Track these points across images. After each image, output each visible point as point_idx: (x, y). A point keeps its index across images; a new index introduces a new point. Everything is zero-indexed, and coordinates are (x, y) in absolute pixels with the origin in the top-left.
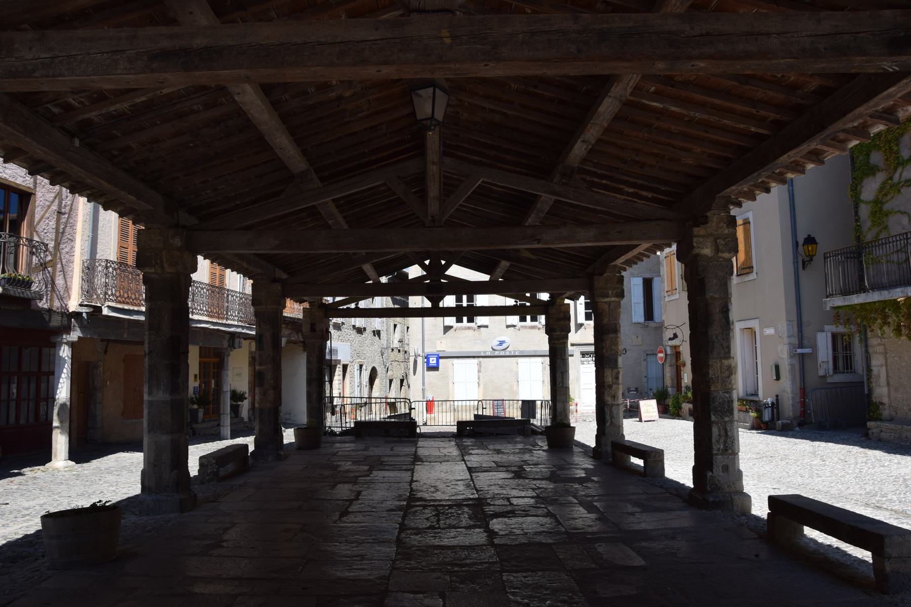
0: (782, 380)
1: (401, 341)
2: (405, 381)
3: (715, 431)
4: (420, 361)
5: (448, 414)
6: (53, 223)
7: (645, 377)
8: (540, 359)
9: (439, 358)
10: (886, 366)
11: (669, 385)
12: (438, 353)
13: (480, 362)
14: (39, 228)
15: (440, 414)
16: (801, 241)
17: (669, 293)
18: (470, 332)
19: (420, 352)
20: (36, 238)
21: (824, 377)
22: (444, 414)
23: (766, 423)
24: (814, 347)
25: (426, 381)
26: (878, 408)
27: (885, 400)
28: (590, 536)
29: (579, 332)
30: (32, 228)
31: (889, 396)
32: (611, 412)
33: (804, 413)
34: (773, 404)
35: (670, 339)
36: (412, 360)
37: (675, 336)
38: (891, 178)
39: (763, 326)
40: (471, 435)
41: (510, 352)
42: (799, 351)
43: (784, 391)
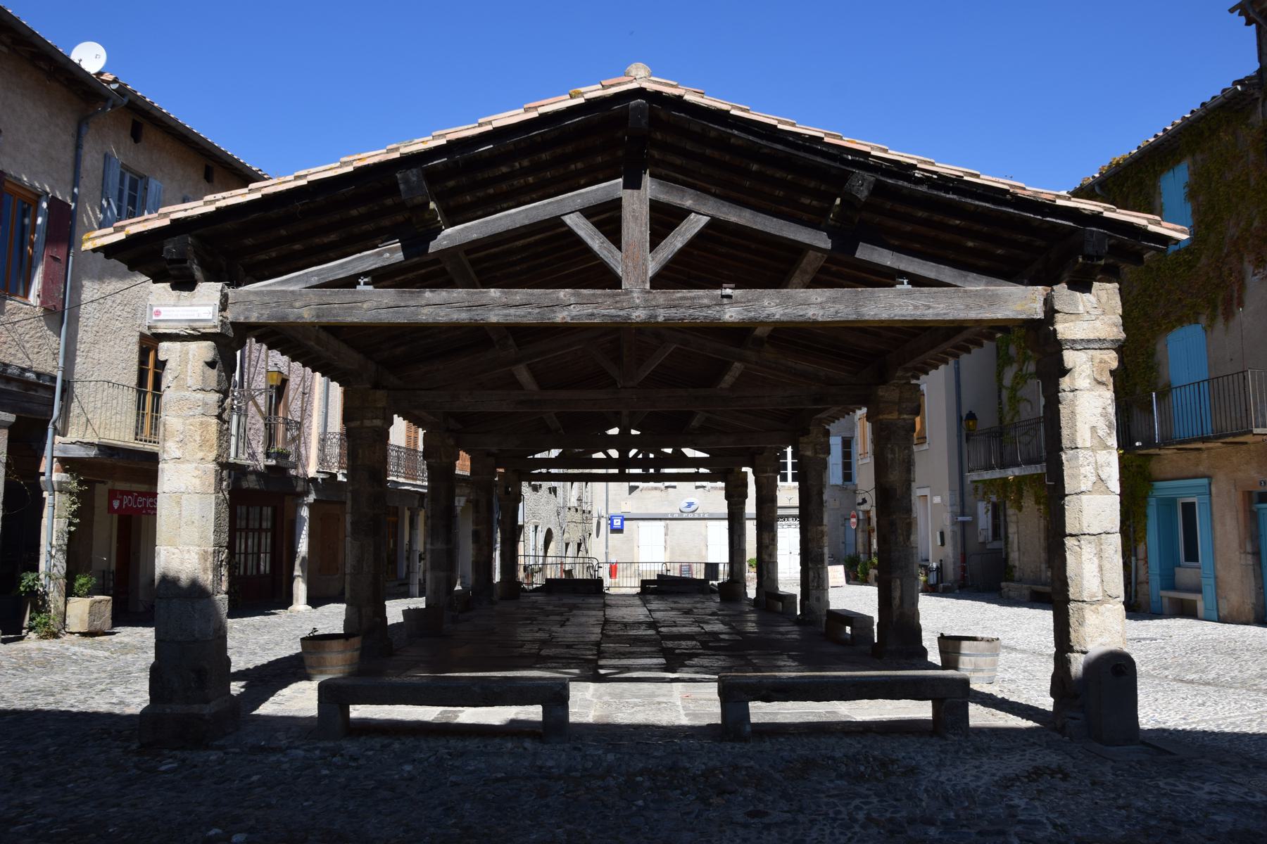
0: (946, 546)
1: (579, 500)
2: (583, 545)
4: (603, 522)
5: (633, 579)
6: (299, 403)
7: (843, 543)
8: (752, 521)
9: (624, 519)
10: (1018, 533)
11: (861, 551)
13: (667, 525)
14: (291, 409)
15: (625, 579)
16: (964, 417)
17: (862, 456)
18: (657, 493)
19: (604, 513)
20: (290, 417)
21: (984, 543)
22: (629, 579)
23: (931, 586)
24: (975, 515)
25: (609, 544)
26: (1012, 571)
27: (1017, 564)
28: (354, 212)
30: (286, 407)
31: (1019, 560)
32: (767, 567)
33: (963, 577)
34: (937, 568)
36: (595, 521)
37: (864, 501)
38: (1021, 370)
39: (933, 495)
40: (653, 592)
41: (699, 514)
42: (960, 519)
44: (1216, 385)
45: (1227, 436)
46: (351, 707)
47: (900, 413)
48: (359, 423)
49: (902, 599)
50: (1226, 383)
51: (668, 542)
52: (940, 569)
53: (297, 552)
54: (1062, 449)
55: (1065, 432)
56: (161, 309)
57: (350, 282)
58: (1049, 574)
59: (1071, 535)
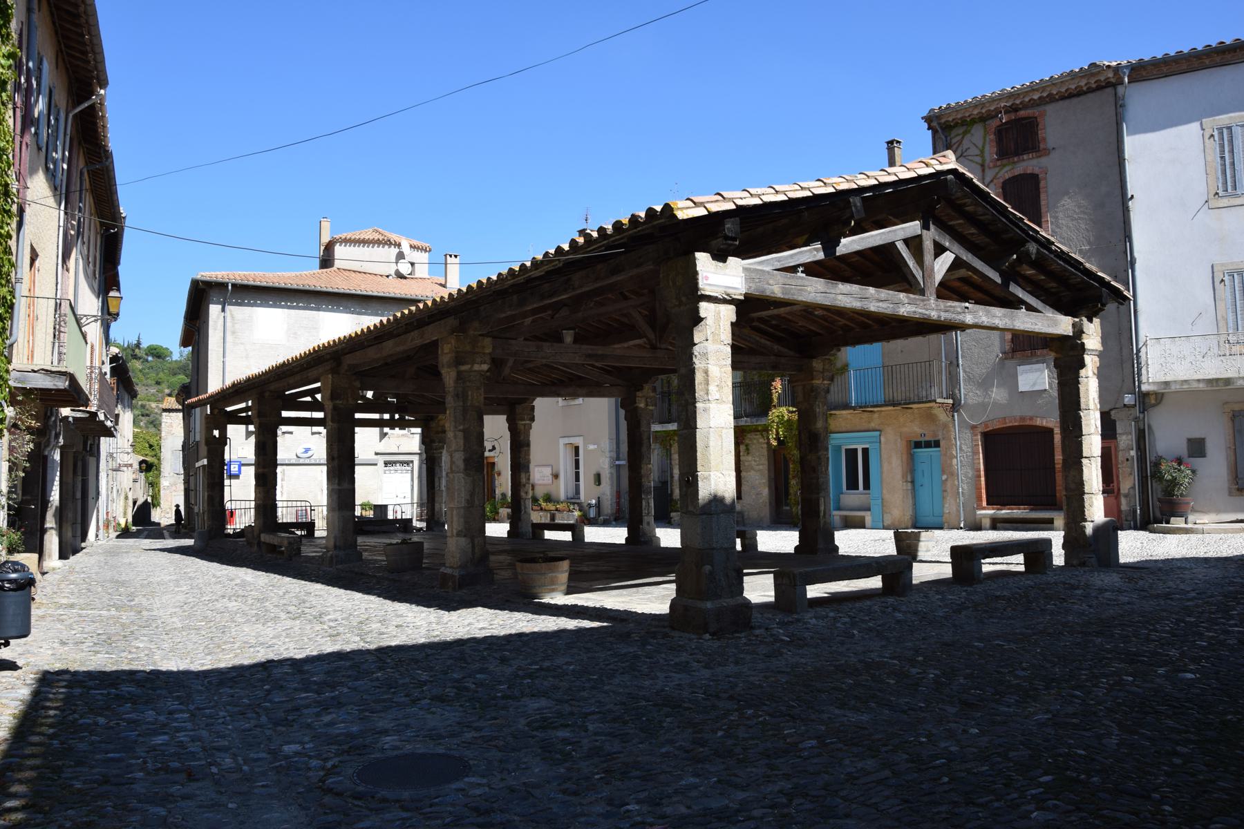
3: (644, 503)
12: (239, 460)
35: (490, 451)
41: (315, 460)
42: (617, 463)
43: (604, 494)
44: (919, 368)
45: (865, 407)
46: (808, 588)
47: (823, 380)
48: (469, 366)
50: (923, 368)
51: (284, 487)
52: (598, 505)
53: (49, 501)
54: (1080, 410)
55: (1082, 400)
56: (709, 275)
57: (792, 269)
58: (231, 532)
59: (1086, 457)
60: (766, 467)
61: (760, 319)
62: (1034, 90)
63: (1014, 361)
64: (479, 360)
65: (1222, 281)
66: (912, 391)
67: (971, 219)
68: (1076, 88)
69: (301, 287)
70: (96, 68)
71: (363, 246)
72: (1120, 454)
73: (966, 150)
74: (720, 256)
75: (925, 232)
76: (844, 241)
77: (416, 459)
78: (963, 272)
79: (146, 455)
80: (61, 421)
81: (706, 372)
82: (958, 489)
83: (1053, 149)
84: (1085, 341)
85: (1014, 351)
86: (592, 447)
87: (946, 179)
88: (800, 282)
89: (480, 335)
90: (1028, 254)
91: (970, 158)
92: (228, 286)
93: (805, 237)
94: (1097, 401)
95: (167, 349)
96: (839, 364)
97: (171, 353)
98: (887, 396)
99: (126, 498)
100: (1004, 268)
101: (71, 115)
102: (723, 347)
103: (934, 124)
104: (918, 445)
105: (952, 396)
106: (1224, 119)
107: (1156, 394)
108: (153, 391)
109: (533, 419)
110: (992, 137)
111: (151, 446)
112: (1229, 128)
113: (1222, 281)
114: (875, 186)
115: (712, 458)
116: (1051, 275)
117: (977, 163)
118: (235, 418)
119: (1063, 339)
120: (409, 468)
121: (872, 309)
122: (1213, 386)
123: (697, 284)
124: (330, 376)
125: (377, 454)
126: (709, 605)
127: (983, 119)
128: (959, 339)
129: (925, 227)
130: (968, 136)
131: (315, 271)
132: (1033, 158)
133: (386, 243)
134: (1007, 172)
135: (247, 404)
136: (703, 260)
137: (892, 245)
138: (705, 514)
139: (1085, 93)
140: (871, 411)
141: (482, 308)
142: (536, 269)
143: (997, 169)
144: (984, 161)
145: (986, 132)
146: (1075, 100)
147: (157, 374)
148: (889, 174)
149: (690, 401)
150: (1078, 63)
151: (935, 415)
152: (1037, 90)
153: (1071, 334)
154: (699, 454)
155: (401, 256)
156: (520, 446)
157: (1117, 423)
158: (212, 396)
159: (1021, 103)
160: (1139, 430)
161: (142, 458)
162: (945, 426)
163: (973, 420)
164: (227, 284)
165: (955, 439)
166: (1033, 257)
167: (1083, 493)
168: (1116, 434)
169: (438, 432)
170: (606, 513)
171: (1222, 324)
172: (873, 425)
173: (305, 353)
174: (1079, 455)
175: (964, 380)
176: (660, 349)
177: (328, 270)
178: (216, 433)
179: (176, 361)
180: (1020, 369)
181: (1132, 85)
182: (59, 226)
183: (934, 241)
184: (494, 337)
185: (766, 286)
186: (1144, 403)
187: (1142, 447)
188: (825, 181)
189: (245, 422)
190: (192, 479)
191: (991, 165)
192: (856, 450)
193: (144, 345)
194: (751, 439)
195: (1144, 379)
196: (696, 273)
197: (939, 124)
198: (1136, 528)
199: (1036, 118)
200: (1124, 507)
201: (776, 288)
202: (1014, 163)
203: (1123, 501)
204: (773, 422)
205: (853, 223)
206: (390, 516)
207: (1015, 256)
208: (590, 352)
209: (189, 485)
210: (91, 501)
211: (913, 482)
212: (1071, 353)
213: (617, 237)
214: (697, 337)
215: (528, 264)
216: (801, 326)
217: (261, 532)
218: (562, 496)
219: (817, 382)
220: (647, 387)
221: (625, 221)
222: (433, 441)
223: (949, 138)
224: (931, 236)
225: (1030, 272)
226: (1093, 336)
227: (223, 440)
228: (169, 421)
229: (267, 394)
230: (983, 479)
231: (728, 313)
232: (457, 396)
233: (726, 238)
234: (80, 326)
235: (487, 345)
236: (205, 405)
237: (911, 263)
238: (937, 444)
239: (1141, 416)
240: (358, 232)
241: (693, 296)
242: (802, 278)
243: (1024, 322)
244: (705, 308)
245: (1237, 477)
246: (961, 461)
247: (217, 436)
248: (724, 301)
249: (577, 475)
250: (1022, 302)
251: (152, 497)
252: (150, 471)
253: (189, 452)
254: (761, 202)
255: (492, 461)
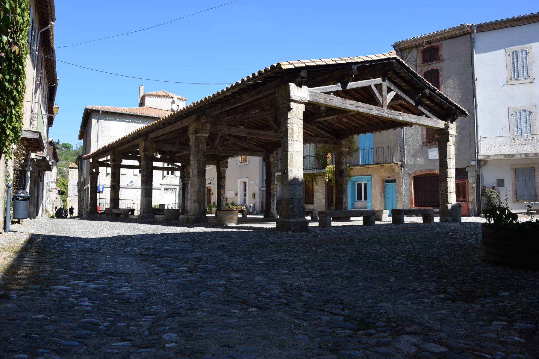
0: (255, 199)
3: (272, 200)
29: (164, 179)
35: (209, 184)
41: (135, 186)
42: (262, 189)
45: (365, 165)
46: (275, 227)
47: (346, 149)
48: (200, 134)
49: (345, 202)
52: (254, 207)
55: (448, 155)
57: (329, 93)
60: (324, 191)
61: (319, 122)
62: (438, 35)
63: (427, 147)
64: (204, 132)
65: (512, 114)
66: (385, 159)
67: (403, 79)
68: (455, 34)
69: (131, 113)
70: (51, 13)
71: (158, 98)
72: (469, 185)
73: (410, 59)
74: (299, 85)
75: (383, 82)
76: (350, 84)
77: (178, 188)
78: (400, 101)
79: (62, 188)
80: (31, 160)
81: (293, 130)
82: (403, 200)
83: (445, 59)
84: (449, 131)
85: (427, 142)
86: (252, 182)
87: (392, 61)
88: (331, 98)
89: (205, 122)
90: (425, 93)
91: (411, 63)
92: (100, 112)
93: (334, 82)
94: (454, 155)
95: (71, 145)
96: (355, 148)
97: (73, 146)
98: (374, 161)
99: (53, 204)
100: (416, 99)
101: (40, 33)
102: (299, 120)
103: (397, 48)
104: (387, 181)
105: (401, 161)
106: (514, 48)
107: (484, 161)
108: (64, 163)
109: (227, 167)
110: (420, 54)
111: (64, 184)
112: (516, 52)
113: (512, 114)
114: (362, 62)
115: (294, 163)
116: (436, 104)
117: (414, 65)
118: (102, 164)
119: (441, 130)
120: (175, 191)
121: (361, 111)
122: (507, 157)
123: (290, 95)
124: (144, 142)
125: (161, 185)
126: (291, 220)
127: (417, 47)
128: (405, 137)
129: (384, 80)
130: (411, 53)
131: (137, 108)
132: (437, 63)
133: (167, 97)
134: (426, 69)
135: (107, 158)
136: (292, 86)
137: (370, 86)
138: (291, 185)
139: (458, 36)
140: (368, 167)
141: (206, 111)
142: (228, 92)
143: (422, 67)
144: (417, 64)
145: (418, 52)
146: (454, 39)
147: (66, 156)
148: (368, 57)
149: (286, 141)
150: (456, 24)
151: (394, 169)
152: (439, 35)
153: (444, 128)
154: (289, 161)
155: (173, 102)
156: (221, 178)
157: (468, 173)
158: (93, 154)
159: (432, 40)
160: (477, 175)
161: (59, 189)
162: (398, 173)
163: (409, 171)
164: (100, 111)
165: (402, 179)
166: (428, 95)
167: (447, 192)
168: (468, 177)
169: (187, 173)
170: (257, 210)
171: (512, 132)
172: (368, 173)
173: (134, 132)
174: (446, 177)
175: (407, 155)
176: (279, 132)
177: (142, 107)
178: (94, 170)
179: (74, 150)
180: (429, 150)
181: (477, 33)
182: (34, 77)
183: (387, 86)
184: (211, 124)
185: (318, 99)
186: (479, 165)
187: (478, 182)
188: (342, 58)
189: (107, 166)
190: (82, 196)
191: (420, 66)
192: (362, 183)
193: (61, 143)
194: (318, 179)
195: (479, 154)
196: (289, 91)
197: (399, 48)
198: (475, 216)
199: (438, 46)
200: (470, 207)
201: (322, 99)
202: (429, 65)
203: (470, 205)
204: (327, 171)
205: (353, 76)
206: (166, 208)
207: (420, 94)
208: (250, 132)
209: (80, 199)
210: (40, 201)
211: (384, 197)
212: (444, 136)
213: (260, 77)
214: (290, 116)
215: (225, 90)
216: (338, 126)
217: (112, 209)
218: (239, 203)
219: (343, 149)
220: (274, 153)
221: (263, 70)
222: (185, 177)
223: (402, 54)
224: (386, 84)
225: (428, 102)
226: (453, 129)
227: (97, 173)
228: (72, 173)
229: (116, 152)
230: (413, 196)
231: (302, 108)
232: (195, 146)
233: (302, 78)
234: (42, 115)
235: (208, 126)
236: (90, 158)
237: (377, 94)
238: (395, 181)
239: (478, 170)
240: (155, 92)
241: (288, 100)
242: (332, 97)
243: (424, 121)
244: (293, 105)
245: (516, 195)
246: (404, 188)
247: (95, 172)
248: (300, 103)
249: (245, 194)
250: (424, 114)
251: (64, 206)
252: (63, 195)
253: (81, 184)
254: (316, 65)
255: (210, 188)
